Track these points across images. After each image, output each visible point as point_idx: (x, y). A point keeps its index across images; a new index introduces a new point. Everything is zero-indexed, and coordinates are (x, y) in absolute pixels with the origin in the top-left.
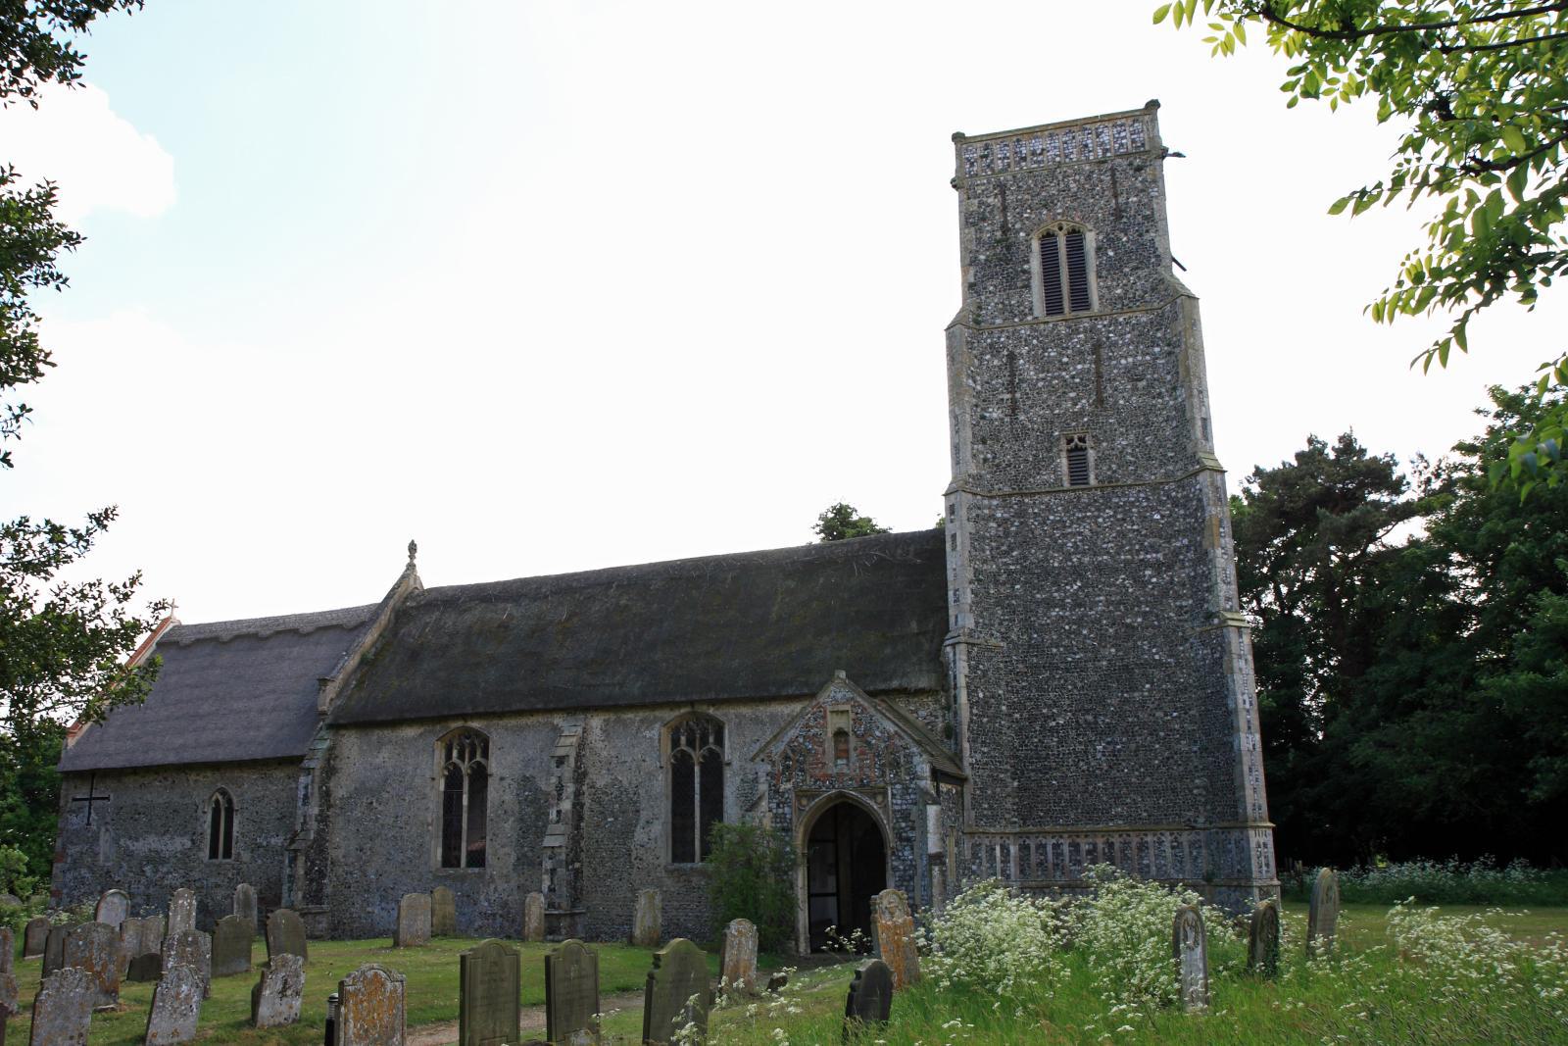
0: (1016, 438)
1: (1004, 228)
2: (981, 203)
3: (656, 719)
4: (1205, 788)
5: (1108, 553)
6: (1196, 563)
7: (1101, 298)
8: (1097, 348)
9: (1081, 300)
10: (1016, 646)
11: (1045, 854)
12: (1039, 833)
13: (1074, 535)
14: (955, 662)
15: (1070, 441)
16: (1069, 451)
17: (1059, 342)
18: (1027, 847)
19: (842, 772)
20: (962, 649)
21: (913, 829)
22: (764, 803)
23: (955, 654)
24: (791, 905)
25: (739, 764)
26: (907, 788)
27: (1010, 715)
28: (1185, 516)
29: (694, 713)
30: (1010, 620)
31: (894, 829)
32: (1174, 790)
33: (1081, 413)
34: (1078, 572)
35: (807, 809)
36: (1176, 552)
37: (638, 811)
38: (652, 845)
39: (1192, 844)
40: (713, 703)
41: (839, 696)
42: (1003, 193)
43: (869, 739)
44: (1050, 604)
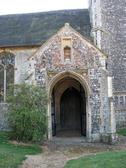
10: (113, 34)
11: (123, 100)
12: (121, 93)
14: (96, 36)
18: (117, 98)
20: (99, 32)
21: (99, 87)
22: (33, 77)
23: (96, 34)
24: (45, 119)
25: (20, 69)
26: (97, 70)
27: (112, 56)
29: (5, 52)
30: (111, 26)
31: (91, 87)
35: (52, 79)
41: (67, 33)
43: (80, 50)
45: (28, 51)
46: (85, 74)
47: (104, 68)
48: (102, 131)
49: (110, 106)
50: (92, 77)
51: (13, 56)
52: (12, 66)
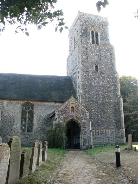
0: (88, 62)
1: (86, 28)
2: (82, 23)
3: (19, 103)
4: (115, 123)
5: (101, 84)
6: (114, 88)
7: (101, 43)
8: (100, 51)
9: (97, 43)
13: (96, 80)
14: (79, 98)
15: (95, 65)
16: (95, 66)
17: (94, 48)
19: (74, 115)
20: (80, 96)
21: (86, 126)
23: (79, 97)
28: (112, 80)
32: (110, 123)
33: (97, 61)
34: (97, 86)
36: (111, 85)
37: (14, 121)
38: (17, 128)
39: (113, 131)
40: (31, 100)
42: (86, 23)
44: (92, 91)
45: (42, 103)
46: (80, 120)
47: (88, 118)
48: (87, 145)
49: (91, 134)
50: (83, 121)
51: (32, 106)
52: (32, 111)
